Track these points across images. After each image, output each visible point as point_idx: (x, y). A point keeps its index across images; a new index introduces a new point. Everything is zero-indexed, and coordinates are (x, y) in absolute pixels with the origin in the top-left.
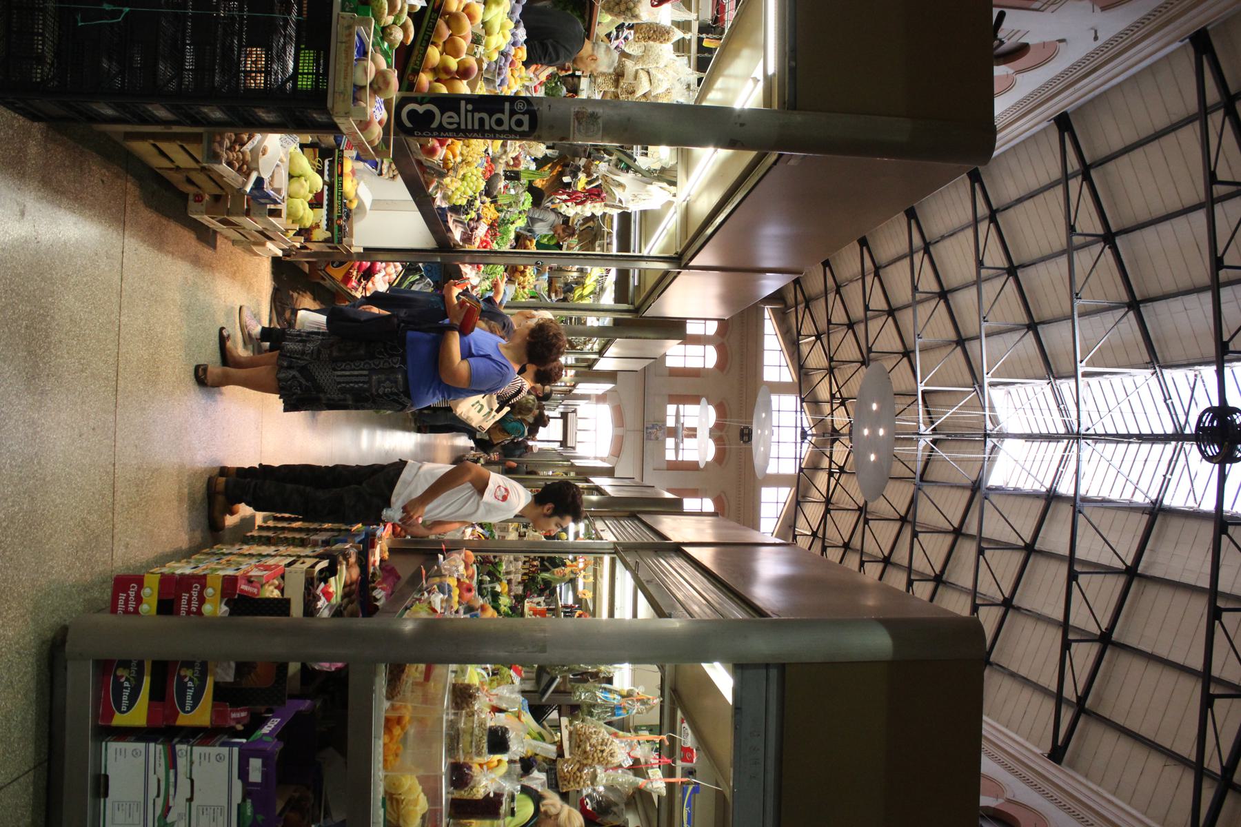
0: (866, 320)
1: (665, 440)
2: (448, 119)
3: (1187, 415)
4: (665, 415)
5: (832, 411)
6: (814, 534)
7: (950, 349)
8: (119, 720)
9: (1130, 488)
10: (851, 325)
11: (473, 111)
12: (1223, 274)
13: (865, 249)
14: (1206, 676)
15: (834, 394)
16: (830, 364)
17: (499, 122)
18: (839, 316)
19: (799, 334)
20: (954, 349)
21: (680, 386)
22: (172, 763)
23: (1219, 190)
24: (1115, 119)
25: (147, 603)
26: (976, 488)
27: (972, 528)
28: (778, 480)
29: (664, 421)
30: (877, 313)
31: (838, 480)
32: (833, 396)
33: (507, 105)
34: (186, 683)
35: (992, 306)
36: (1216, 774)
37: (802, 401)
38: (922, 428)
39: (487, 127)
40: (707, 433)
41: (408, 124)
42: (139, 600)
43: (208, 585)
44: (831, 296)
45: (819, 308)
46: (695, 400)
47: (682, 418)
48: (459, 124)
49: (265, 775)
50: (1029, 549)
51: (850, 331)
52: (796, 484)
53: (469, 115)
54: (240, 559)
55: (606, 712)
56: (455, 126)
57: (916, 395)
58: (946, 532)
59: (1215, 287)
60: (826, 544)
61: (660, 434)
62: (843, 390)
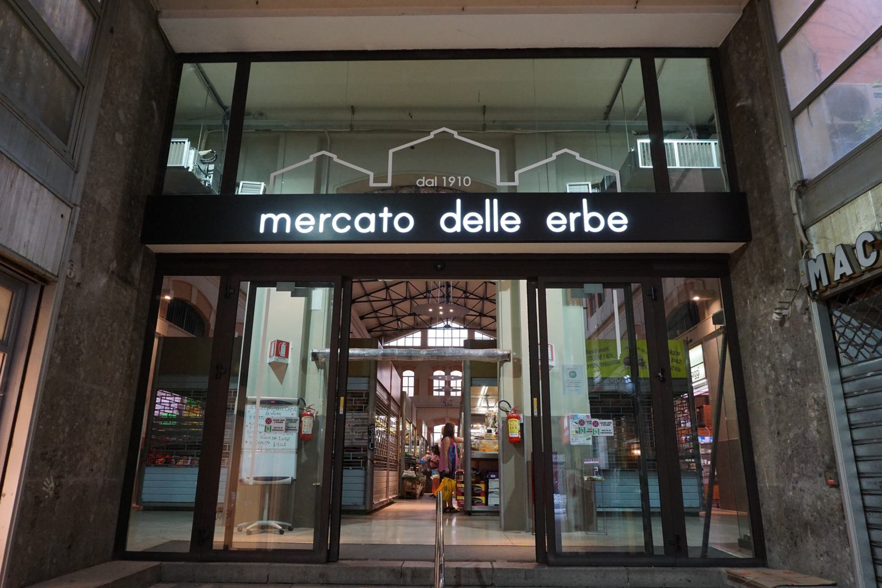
0: (391, 300)
1: (452, 396)
4: (439, 396)
5: (433, 297)
8: (484, 502)
10: (393, 305)
13: (357, 300)
15: (425, 296)
16: (409, 299)
18: (389, 311)
22: (492, 492)
24: (285, 152)
32: (425, 297)
44: (371, 298)
47: (440, 388)
51: (396, 305)
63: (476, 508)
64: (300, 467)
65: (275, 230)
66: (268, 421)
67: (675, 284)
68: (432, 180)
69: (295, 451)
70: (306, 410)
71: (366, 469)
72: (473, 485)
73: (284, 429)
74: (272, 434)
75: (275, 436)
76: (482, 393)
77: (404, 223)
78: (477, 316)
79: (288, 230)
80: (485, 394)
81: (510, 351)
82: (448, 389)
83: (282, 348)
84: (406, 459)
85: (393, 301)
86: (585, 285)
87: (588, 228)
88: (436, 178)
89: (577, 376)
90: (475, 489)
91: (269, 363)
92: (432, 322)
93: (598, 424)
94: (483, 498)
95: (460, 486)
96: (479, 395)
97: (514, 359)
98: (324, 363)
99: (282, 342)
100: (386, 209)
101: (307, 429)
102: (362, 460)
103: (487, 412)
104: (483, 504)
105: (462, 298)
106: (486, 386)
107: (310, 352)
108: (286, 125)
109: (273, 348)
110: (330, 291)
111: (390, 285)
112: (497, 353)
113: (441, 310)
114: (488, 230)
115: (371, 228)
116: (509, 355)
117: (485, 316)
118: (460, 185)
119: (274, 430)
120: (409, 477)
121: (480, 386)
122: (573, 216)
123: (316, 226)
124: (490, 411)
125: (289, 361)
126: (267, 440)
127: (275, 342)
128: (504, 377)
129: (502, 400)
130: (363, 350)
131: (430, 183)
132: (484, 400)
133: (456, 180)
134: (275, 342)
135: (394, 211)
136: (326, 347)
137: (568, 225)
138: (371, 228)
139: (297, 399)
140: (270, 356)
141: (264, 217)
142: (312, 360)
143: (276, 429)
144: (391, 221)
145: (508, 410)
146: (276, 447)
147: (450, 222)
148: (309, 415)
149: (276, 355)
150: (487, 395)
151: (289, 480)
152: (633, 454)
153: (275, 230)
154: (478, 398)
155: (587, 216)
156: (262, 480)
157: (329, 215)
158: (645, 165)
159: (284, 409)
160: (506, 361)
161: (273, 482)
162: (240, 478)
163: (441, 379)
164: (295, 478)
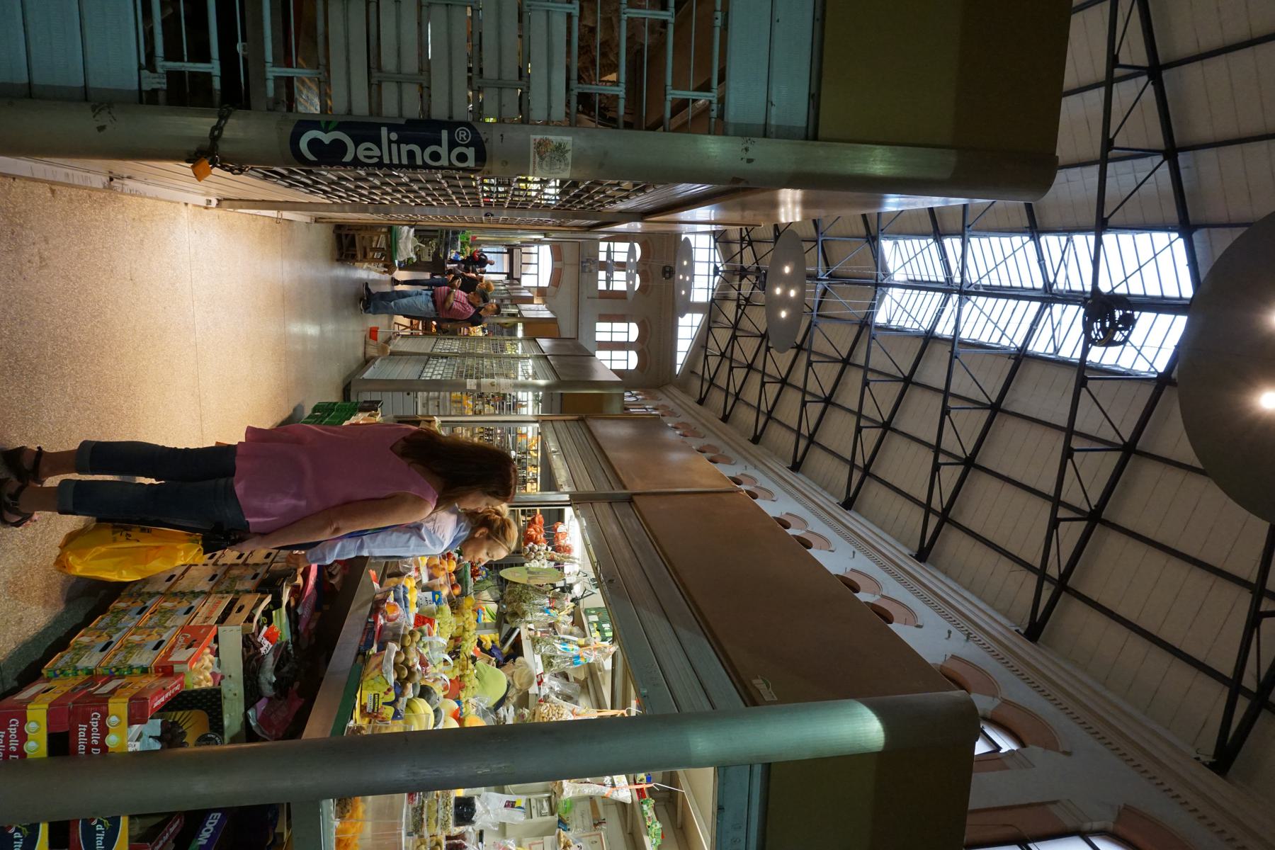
2: (365, 151)
3: (1056, 275)
5: (742, 249)
6: (723, 355)
9: (998, 334)
11: (398, 142)
12: (1112, 153)
14: (937, 449)
17: (436, 156)
23: (1118, 72)
25: (33, 740)
26: (865, 324)
27: (860, 359)
28: (696, 308)
31: (743, 310)
32: (742, 239)
33: (445, 134)
34: (95, 826)
36: (1054, 579)
37: (716, 241)
38: (821, 273)
39: (419, 162)
41: (311, 157)
42: (22, 737)
43: (110, 713)
48: (381, 158)
50: (908, 381)
52: (708, 311)
53: (394, 147)
54: (168, 605)
55: (565, 662)
56: (376, 160)
59: (1103, 162)
71: (148, 98)
82: (610, 266)
84: (447, 233)
102: (214, 67)
120: (396, 243)
163: (628, 285)
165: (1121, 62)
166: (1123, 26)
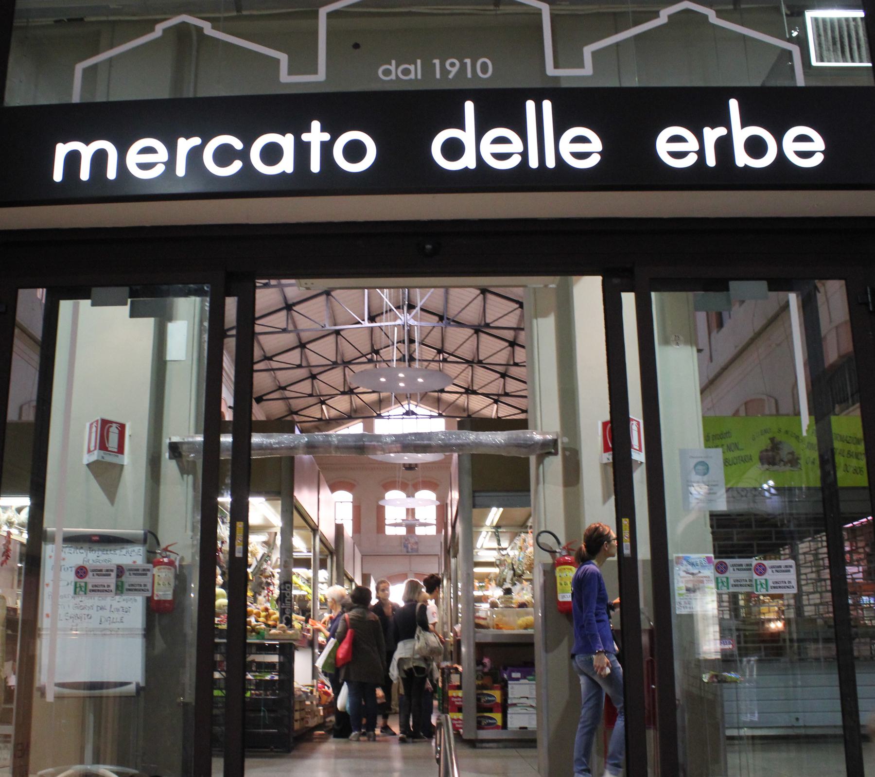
0: (309, 366)
1: (418, 536)
6: (496, 402)
7: (335, 303)
8: (499, 723)
11: (285, 603)
16: (340, 364)
18: (305, 387)
19: (320, 420)
20: (332, 296)
21: (369, 522)
22: (515, 705)
29: (401, 537)
30: (303, 357)
32: (370, 361)
35: (316, 322)
38: (399, 322)
40: (410, 500)
44: (288, 394)
45: (296, 404)
46: (381, 510)
49: (518, 672)
57: (372, 328)
58: (485, 299)
60: (503, 393)
61: (412, 540)
62: (364, 352)
63: (484, 734)
64: (152, 664)
65: (85, 174)
66: (81, 572)
67: (831, 321)
68: (412, 67)
69: (141, 632)
70: (160, 554)
72: (480, 692)
73: (113, 587)
74: (92, 601)
75: (102, 603)
76: (488, 522)
77: (355, 151)
78: (461, 393)
79: (112, 173)
80: (495, 524)
81: (557, 435)
83: (111, 435)
85: (313, 369)
86: (733, 284)
87: (742, 159)
88: (419, 62)
89: (711, 471)
90: (483, 700)
91: (88, 465)
92: (382, 406)
93: (765, 569)
94: (498, 717)
95: (454, 695)
96: (482, 526)
97: (564, 449)
98: (194, 462)
99: (112, 422)
100: (316, 125)
101: (164, 592)
103: (499, 557)
104: (497, 727)
105: (436, 361)
106: (498, 506)
107: (166, 442)
108: (111, 7)
109: (93, 435)
110: (202, 302)
111: (306, 341)
112: (532, 439)
113: (401, 380)
114: (534, 163)
115: (287, 165)
116: (555, 442)
117: (475, 393)
118: (469, 75)
119: (93, 591)
121: (489, 507)
122: (711, 135)
123: (171, 164)
124: (504, 555)
125: (126, 459)
126: (86, 612)
127: (97, 424)
128: (546, 484)
129: (543, 529)
130: (268, 437)
131: (406, 72)
132: (491, 536)
133: (460, 68)
134: (97, 424)
135: (334, 129)
136: (197, 432)
137: (701, 153)
138: (287, 165)
139: (142, 532)
140: (89, 451)
141: (62, 150)
142: (170, 458)
143: (97, 590)
144: (327, 148)
145: (554, 549)
146: (106, 625)
147: (453, 149)
148: (166, 564)
149: (101, 449)
150: (498, 527)
151: (132, 688)
152: (768, 629)
153: (85, 174)
154: (481, 532)
155: (741, 135)
156: (84, 689)
157: (196, 141)
158: (822, 60)
159: (118, 552)
160: (550, 454)
161: (105, 692)
162: (37, 684)
164: (142, 684)
165: (311, 393)
166: (283, 364)
